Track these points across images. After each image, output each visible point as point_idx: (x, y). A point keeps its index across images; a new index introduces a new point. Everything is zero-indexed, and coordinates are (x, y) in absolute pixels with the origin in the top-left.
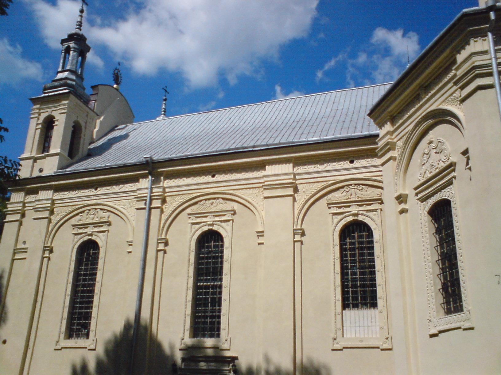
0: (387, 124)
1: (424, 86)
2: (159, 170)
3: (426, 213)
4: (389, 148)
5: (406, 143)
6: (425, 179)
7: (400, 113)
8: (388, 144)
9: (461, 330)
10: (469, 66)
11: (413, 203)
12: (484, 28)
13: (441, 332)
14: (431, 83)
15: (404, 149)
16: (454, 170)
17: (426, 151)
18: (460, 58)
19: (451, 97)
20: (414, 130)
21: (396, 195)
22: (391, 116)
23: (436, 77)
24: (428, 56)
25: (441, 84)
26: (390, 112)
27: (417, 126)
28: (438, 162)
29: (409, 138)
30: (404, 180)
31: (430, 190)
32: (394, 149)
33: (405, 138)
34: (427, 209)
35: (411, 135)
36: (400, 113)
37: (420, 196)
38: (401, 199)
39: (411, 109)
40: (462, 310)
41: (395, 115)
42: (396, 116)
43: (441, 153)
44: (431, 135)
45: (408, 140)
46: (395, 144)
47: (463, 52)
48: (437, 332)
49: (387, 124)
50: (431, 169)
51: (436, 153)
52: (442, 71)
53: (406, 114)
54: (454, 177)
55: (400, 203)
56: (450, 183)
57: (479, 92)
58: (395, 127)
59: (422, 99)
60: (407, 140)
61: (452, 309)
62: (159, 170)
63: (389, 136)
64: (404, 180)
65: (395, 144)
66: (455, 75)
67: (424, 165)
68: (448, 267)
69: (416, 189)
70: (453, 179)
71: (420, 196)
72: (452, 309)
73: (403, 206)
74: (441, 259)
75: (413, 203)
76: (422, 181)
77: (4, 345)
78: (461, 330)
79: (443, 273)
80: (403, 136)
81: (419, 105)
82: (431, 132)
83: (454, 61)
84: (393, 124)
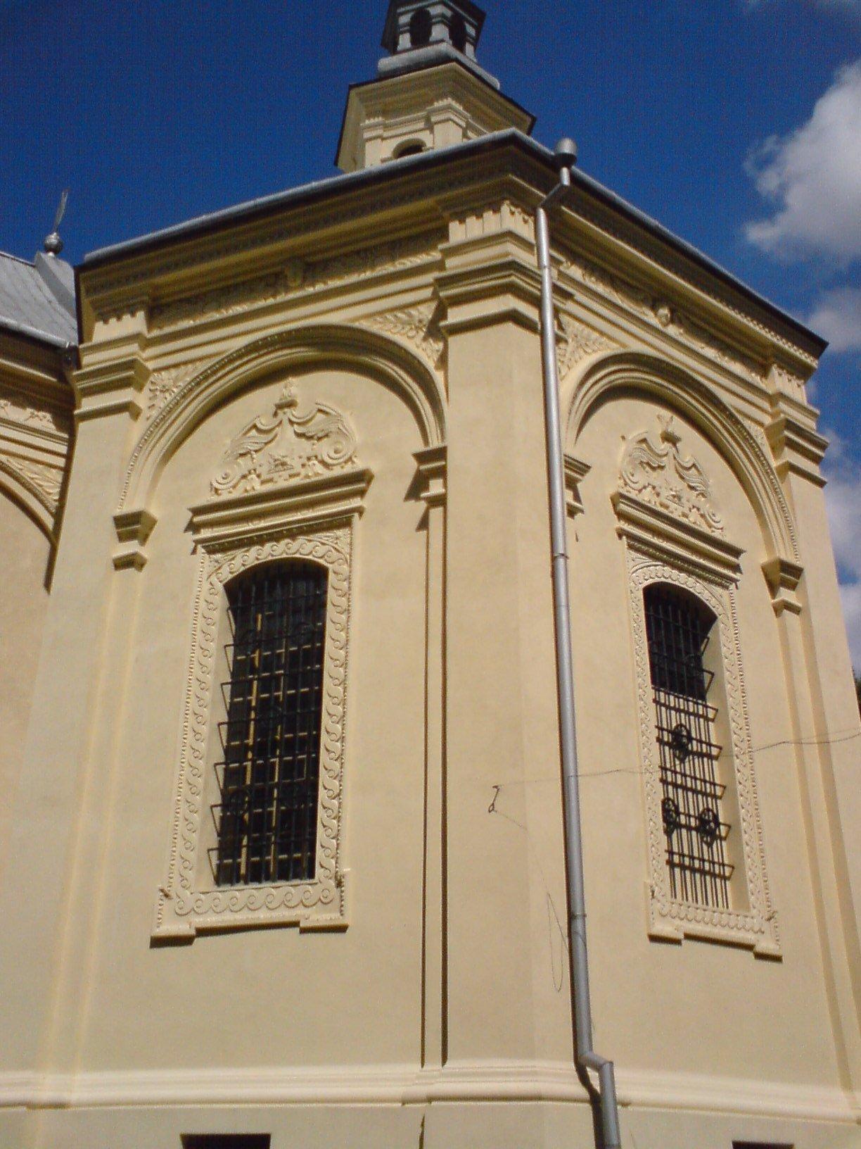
0: (133, 314)
1: (310, 259)
2: (564, 208)
3: (220, 587)
4: (128, 378)
5: (198, 384)
6: (237, 494)
7: (188, 301)
8: (130, 365)
9: (298, 930)
10: (462, 266)
11: (170, 543)
12: (533, 193)
13: (203, 932)
14: (334, 259)
15: (184, 397)
16: (362, 493)
17: (264, 423)
18: (458, 232)
19: (400, 315)
20: (240, 357)
21: (119, 512)
22: (154, 299)
23: (358, 252)
24: (336, 199)
25: (368, 274)
26: (157, 287)
27: (253, 348)
28: (299, 461)
29: (214, 373)
30: (155, 479)
31: (251, 526)
32: (140, 388)
33: (202, 367)
34: (226, 575)
35: (223, 367)
36: (188, 301)
37: (206, 533)
38: (132, 525)
39: (239, 302)
40: (311, 875)
41: (164, 301)
42: (168, 305)
43: (319, 439)
44: (294, 386)
45: (206, 378)
46: (145, 374)
47: (472, 221)
48: (193, 932)
49: (133, 314)
50: (269, 472)
51: (299, 435)
52: (382, 245)
53: (218, 309)
54: (360, 511)
55: (122, 538)
56: (342, 521)
57: (510, 327)
58: (156, 333)
59: (288, 289)
60: (205, 376)
61: (243, 871)
62: (564, 208)
63: (134, 347)
64: (155, 479)
65: (145, 374)
66: (440, 265)
67: (242, 455)
68: (252, 749)
69: (197, 511)
70: (356, 515)
71: (206, 533)
72: (243, 871)
73: (131, 547)
74: (229, 724)
75: (170, 543)
76: (225, 497)
77: (807, 574)
78: (298, 930)
79: (226, 763)
80: (201, 359)
81: (271, 301)
82: (291, 380)
83: (443, 234)
84: (151, 320)
